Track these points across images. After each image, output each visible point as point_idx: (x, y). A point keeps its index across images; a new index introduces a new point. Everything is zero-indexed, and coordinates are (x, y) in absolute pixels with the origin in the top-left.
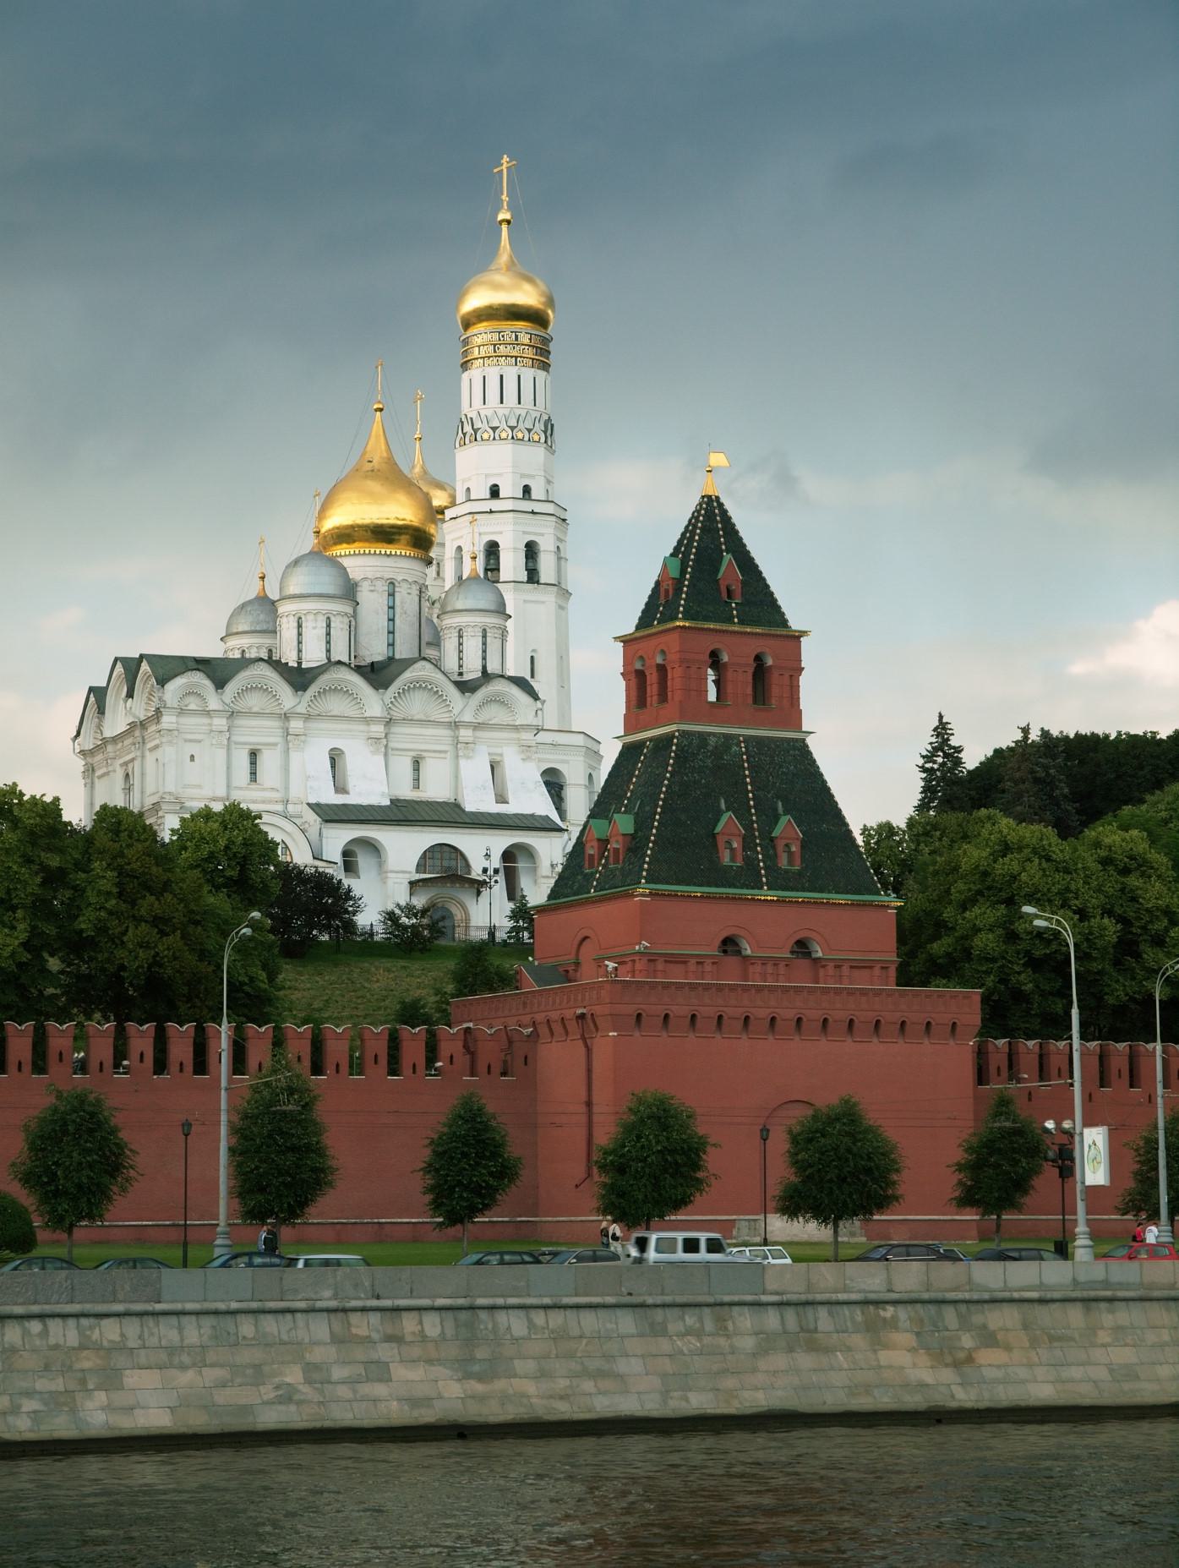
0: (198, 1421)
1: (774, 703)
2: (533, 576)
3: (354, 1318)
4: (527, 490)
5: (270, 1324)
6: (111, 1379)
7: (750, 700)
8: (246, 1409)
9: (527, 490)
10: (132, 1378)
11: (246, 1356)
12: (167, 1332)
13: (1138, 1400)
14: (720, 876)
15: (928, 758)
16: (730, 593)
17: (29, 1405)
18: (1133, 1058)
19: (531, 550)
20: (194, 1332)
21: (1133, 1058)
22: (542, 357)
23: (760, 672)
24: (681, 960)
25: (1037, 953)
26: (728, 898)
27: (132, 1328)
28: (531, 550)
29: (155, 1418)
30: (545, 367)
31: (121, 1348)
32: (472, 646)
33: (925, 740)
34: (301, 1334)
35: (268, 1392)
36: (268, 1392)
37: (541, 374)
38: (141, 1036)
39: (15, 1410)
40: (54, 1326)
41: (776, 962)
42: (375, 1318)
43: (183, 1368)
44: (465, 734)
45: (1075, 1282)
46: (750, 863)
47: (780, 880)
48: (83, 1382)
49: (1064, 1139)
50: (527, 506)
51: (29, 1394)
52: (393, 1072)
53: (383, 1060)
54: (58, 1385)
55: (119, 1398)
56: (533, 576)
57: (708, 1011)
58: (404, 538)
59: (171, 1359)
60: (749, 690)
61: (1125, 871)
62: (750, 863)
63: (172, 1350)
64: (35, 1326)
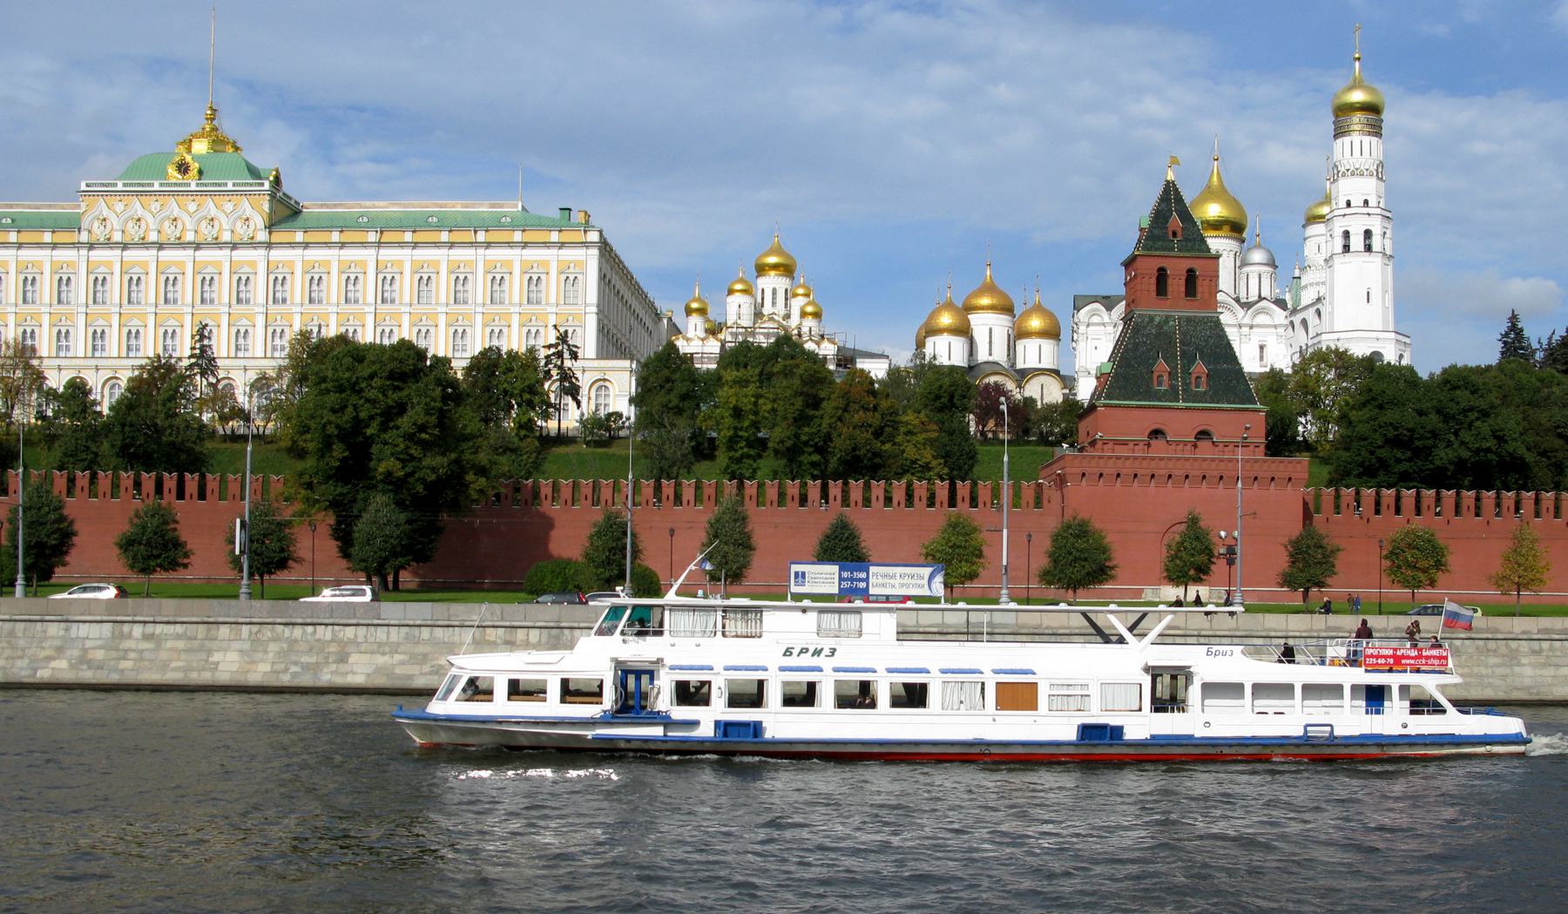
0: (381, 681)
1: (1199, 296)
2: (1368, 248)
3: (488, 631)
4: (1366, 202)
5: (439, 632)
6: (343, 659)
7: (1154, 294)
8: (411, 677)
9: (1366, 202)
10: (353, 659)
11: (420, 649)
12: (381, 634)
13: (1550, 697)
14: (1150, 394)
15: (1506, 335)
16: (1174, 234)
17: (294, 669)
18: (1398, 498)
19: (1368, 234)
20: (395, 635)
21: (1398, 498)
22: (1376, 130)
23: (1191, 277)
24: (1125, 443)
25: (1390, 435)
26: (1154, 407)
27: (362, 631)
28: (1368, 234)
29: (358, 680)
30: (1378, 134)
31: (354, 642)
32: (1254, 282)
33: (1504, 326)
34: (456, 639)
35: (426, 668)
36: (426, 668)
37: (1374, 140)
38: (814, 488)
39: (286, 670)
40: (320, 629)
41: (1185, 444)
42: (501, 631)
43: (384, 654)
44: (1245, 330)
45: (918, 625)
46: (1174, 389)
47: (1191, 396)
48: (326, 658)
49: (1232, 542)
50: (1366, 210)
51: (296, 663)
52: (1477, 515)
53: (924, 500)
54: (313, 659)
55: (343, 668)
56: (1368, 248)
57: (1127, 471)
58: (1226, 228)
59: (380, 648)
60: (1154, 288)
61: (1455, 388)
62: (1174, 389)
63: (380, 644)
64: (310, 629)
